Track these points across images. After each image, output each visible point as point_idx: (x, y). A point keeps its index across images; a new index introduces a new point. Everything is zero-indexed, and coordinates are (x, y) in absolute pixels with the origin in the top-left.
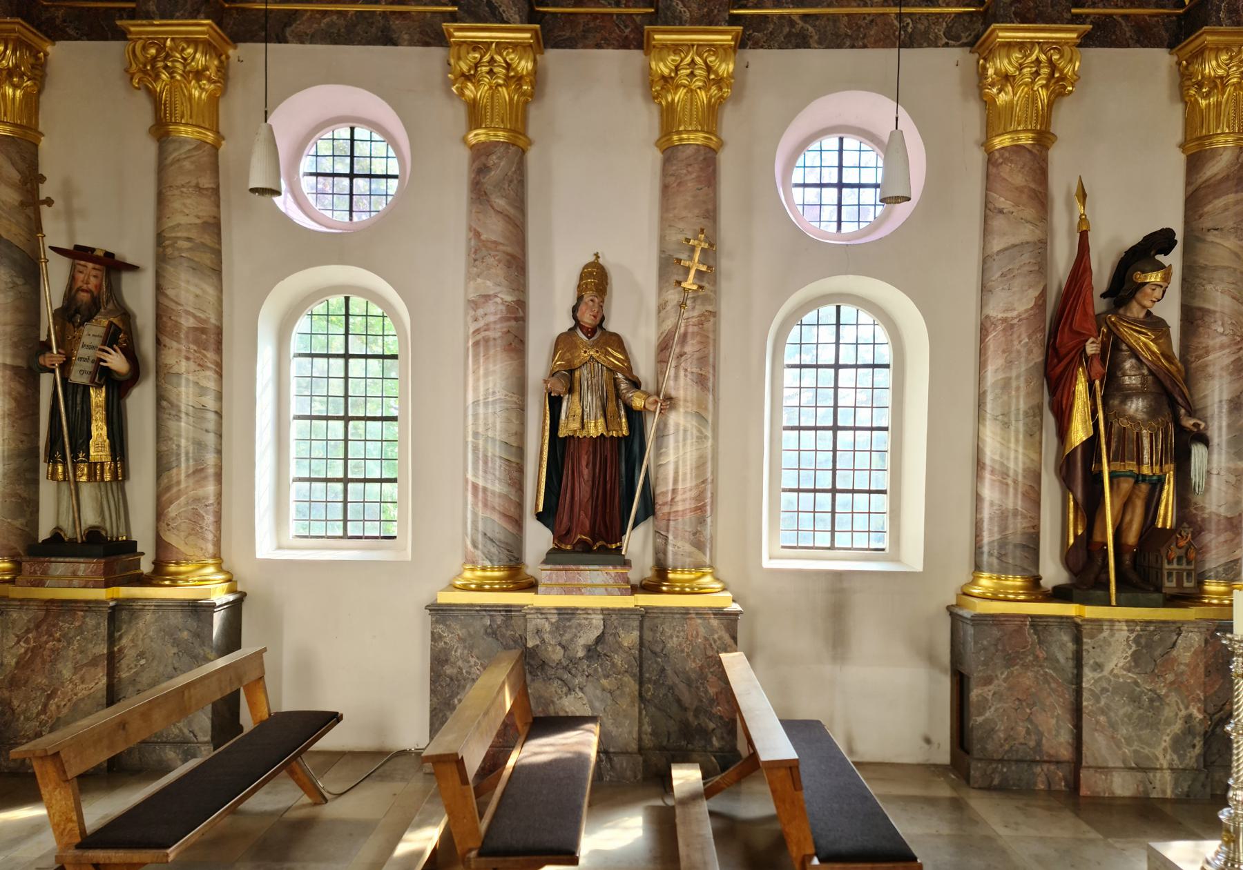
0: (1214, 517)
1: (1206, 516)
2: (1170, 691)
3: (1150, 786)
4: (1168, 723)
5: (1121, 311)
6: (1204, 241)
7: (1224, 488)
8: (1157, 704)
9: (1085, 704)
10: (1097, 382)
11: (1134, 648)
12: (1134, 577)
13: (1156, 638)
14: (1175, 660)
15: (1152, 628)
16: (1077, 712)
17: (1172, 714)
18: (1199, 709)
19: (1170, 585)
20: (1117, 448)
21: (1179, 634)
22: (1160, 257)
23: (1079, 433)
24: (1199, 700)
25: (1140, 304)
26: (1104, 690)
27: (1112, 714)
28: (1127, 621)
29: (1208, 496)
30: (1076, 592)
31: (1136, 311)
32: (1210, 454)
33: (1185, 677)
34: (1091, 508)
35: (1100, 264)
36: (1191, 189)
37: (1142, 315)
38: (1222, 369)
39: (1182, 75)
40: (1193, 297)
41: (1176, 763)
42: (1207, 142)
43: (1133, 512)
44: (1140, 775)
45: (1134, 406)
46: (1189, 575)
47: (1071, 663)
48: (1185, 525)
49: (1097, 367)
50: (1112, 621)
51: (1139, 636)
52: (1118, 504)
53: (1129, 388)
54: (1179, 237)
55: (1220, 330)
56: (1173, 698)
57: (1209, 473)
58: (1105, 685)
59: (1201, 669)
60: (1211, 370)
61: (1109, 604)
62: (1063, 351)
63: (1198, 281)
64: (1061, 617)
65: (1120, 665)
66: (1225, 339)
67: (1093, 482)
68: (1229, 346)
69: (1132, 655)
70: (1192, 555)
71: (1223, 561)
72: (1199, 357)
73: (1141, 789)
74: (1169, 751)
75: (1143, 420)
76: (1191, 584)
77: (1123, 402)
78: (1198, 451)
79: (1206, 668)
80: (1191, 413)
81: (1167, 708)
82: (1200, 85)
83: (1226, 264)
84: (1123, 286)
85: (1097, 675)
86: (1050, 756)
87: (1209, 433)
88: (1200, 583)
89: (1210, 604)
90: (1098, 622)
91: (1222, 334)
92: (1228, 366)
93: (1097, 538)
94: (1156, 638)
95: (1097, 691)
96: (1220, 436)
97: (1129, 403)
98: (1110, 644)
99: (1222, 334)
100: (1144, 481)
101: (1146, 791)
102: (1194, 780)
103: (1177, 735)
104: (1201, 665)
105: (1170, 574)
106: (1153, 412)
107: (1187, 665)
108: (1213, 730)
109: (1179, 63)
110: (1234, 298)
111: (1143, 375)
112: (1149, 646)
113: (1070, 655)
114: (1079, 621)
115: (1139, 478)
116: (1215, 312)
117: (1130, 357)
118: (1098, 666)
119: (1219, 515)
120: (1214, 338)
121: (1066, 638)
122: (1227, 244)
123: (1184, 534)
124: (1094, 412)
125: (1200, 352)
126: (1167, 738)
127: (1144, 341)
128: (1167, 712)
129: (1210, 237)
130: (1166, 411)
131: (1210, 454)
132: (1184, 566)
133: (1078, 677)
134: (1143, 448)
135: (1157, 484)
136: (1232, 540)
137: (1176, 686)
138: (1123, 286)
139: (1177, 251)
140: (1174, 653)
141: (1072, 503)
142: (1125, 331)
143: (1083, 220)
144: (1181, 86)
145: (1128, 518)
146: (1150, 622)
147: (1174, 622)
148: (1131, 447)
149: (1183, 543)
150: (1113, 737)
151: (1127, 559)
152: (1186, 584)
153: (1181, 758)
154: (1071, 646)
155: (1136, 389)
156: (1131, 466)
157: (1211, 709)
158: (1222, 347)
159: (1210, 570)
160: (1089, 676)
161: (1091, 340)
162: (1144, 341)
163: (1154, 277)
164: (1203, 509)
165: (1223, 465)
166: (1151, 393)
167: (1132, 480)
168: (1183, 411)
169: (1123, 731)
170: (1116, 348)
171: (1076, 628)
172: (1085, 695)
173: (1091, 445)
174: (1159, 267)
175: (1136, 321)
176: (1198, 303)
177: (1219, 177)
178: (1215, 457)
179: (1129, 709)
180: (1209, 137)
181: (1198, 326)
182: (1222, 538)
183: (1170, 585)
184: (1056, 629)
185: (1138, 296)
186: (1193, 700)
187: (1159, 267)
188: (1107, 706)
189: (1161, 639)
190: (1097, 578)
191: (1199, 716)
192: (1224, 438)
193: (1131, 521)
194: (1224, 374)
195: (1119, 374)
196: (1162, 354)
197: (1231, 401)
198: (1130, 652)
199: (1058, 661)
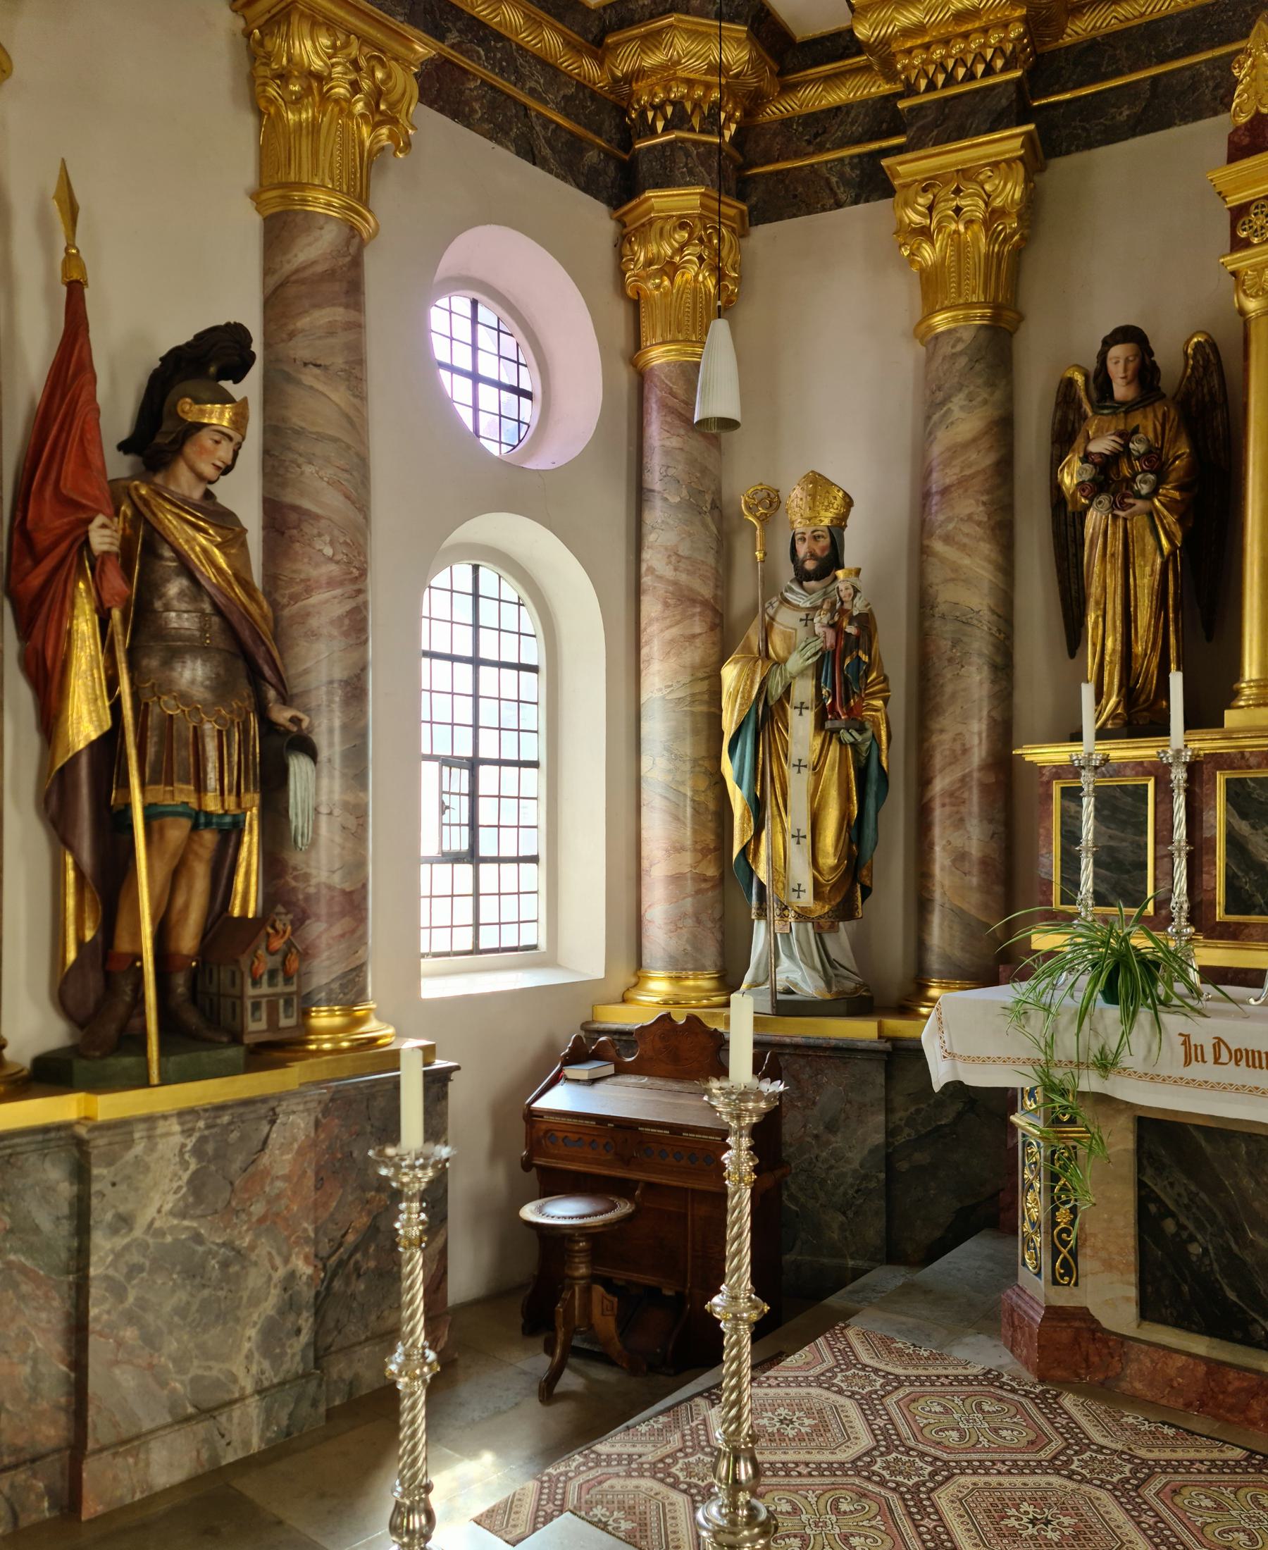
0: (324, 891)
1: (312, 890)
2: (257, 1236)
3: (223, 1442)
4: (255, 1301)
5: (159, 479)
6: (298, 383)
7: (338, 839)
8: (234, 1269)
9: (93, 1312)
10: (116, 614)
11: (193, 1166)
12: (192, 1018)
13: (234, 1136)
14: (266, 1172)
15: (226, 1119)
16: (78, 1331)
17: (261, 1281)
18: (306, 1258)
19: (256, 1027)
20: (158, 755)
21: (273, 1122)
22: (227, 385)
23: (84, 722)
24: (307, 1240)
25: (192, 469)
26: (134, 1270)
27: (150, 1317)
28: (181, 1114)
29: (313, 854)
30: (79, 1065)
31: (184, 483)
32: (318, 777)
33: (284, 1202)
34: (109, 883)
35: (113, 381)
36: (274, 280)
37: (197, 494)
38: (332, 622)
39: (253, 58)
40: (283, 485)
41: (271, 1377)
42: (296, 195)
43: (190, 888)
44: (201, 1428)
45: (187, 674)
46: (288, 1003)
47: (66, 1228)
48: (280, 908)
49: (114, 581)
50: (150, 1120)
51: (203, 1140)
52: (163, 871)
53: (178, 635)
54: (257, 347)
55: (328, 551)
56: (265, 1247)
57: (317, 811)
58: (136, 1258)
59: (310, 1181)
60: (314, 622)
61: (146, 1084)
62: (42, 540)
63: (291, 456)
64: (45, 1129)
65: (167, 1207)
66: (333, 569)
67: (113, 825)
68: (341, 583)
69: (190, 1181)
70: (294, 964)
71: (339, 970)
72: (295, 598)
73: (205, 1455)
74: (256, 1355)
75: (204, 703)
76: (291, 1022)
77: (167, 663)
78: (299, 767)
79: (317, 1173)
80: (286, 699)
81: (253, 1271)
82: (283, 77)
83: (331, 432)
84: (159, 436)
85: (120, 1242)
86: (17, 1450)
87: (315, 738)
88: (306, 1014)
89: (319, 1053)
90: (121, 1127)
91: (331, 559)
92: (340, 618)
93: (123, 944)
94: (234, 1136)
95: (119, 1277)
96: (331, 745)
97: (178, 666)
98: (147, 1169)
99: (331, 559)
100: (208, 824)
101: (214, 1457)
102: (298, 1401)
103: (270, 1318)
104: (310, 1173)
105: (256, 1006)
106: (221, 688)
107: (286, 1178)
108: (328, 1288)
109: (248, 34)
110: (348, 497)
111: (202, 612)
112: (220, 1155)
113: (65, 1210)
114: (82, 1131)
115: (200, 820)
116: (317, 517)
117: (179, 574)
118: (124, 1221)
119: (330, 888)
120: (317, 565)
121: (56, 1175)
122: (335, 397)
123: (279, 926)
124: (112, 683)
125: (296, 589)
126: (252, 1332)
127: (200, 543)
128: (254, 1280)
129: (309, 377)
130: (245, 690)
131: (318, 777)
132: (280, 988)
133: (81, 1255)
134: (205, 759)
135: (231, 832)
136: (353, 931)
137: (268, 1223)
138: (159, 436)
139: (255, 375)
140: (265, 1160)
141: (71, 875)
142: (171, 522)
143: (72, 259)
144: (252, 78)
145: (180, 901)
146: (221, 1108)
147: (264, 1100)
148: (184, 755)
149: (278, 944)
150: (151, 1366)
151: (180, 983)
152: (284, 1022)
153: (276, 1360)
154: (66, 1189)
155: (190, 639)
156: (184, 794)
157: (325, 1249)
158: (332, 583)
159: (319, 989)
160: (102, 1244)
161: (100, 519)
162: (200, 543)
163: (218, 416)
164: (306, 877)
165: (337, 797)
166: (218, 650)
167: (186, 823)
168: (272, 694)
169: (172, 1346)
170: (151, 552)
171: (74, 1147)
172: (95, 1291)
173: (107, 748)
174: (226, 398)
175: (182, 504)
176: (290, 497)
177: (319, 268)
178: (325, 782)
179: (182, 1296)
180: (300, 186)
181: (292, 540)
182: (337, 930)
183: (256, 1027)
184: (33, 1158)
185: (189, 450)
186: (296, 1243)
187: (226, 398)
188: (142, 1303)
189: (241, 1139)
190: (122, 1030)
191: (305, 1270)
192: (338, 748)
193: (187, 906)
194: (335, 633)
195: (158, 605)
196: (236, 575)
197: (346, 683)
198: (186, 1176)
199: (37, 1229)
